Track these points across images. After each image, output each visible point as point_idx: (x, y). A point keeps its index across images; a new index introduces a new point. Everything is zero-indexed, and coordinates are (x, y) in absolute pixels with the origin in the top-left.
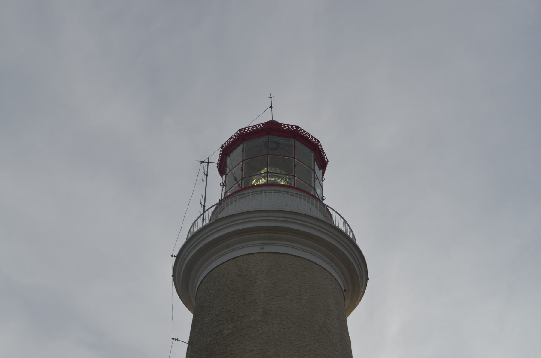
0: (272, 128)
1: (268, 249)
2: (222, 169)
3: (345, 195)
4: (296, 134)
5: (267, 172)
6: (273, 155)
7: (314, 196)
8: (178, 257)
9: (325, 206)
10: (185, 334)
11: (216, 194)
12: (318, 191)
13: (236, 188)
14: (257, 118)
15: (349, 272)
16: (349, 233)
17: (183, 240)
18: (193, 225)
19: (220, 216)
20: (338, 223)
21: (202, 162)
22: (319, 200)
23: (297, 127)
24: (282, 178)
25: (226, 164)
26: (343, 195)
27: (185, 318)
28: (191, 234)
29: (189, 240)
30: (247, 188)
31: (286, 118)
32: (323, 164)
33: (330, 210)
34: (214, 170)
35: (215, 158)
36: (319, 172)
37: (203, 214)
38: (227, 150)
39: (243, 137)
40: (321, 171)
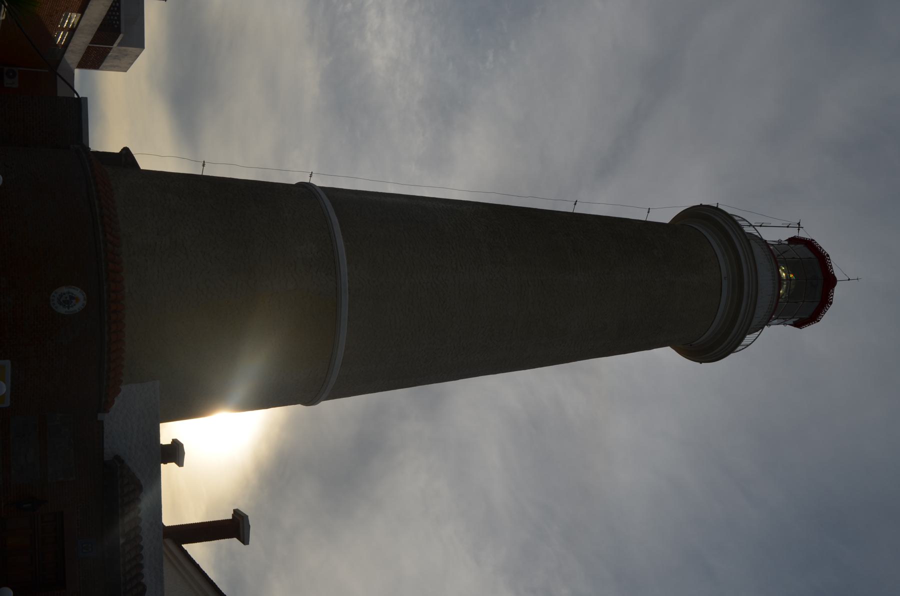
0: (830, 281)
1: (725, 284)
2: (793, 240)
3: (772, 344)
4: (824, 302)
5: (790, 279)
6: (805, 284)
7: (771, 318)
8: (717, 208)
9: (762, 328)
10: (653, 218)
11: (770, 235)
12: (776, 321)
13: (776, 253)
14: (839, 266)
15: (707, 347)
16: (740, 348)
17: (729, 211)
18: (744, 220)
19: (752, 242)
20: (749, 338)
21: (799, 224)
22: (768, 323)
23: (831, 303)
24: (786, 291)
25: (798, 243)
26: (773, 341)
27: (666, 217)
28: (736, 218)
29: (730, 217)
30: (777, 263)
31: (838, 292)
32: (799, 324)
33: (758, 333)
34: (792, 233)
35: (803, 234)
36: (791, 322)
37: (751, 225)
38: (810, 244)
39: (820, 258)
40: (79, 15)
